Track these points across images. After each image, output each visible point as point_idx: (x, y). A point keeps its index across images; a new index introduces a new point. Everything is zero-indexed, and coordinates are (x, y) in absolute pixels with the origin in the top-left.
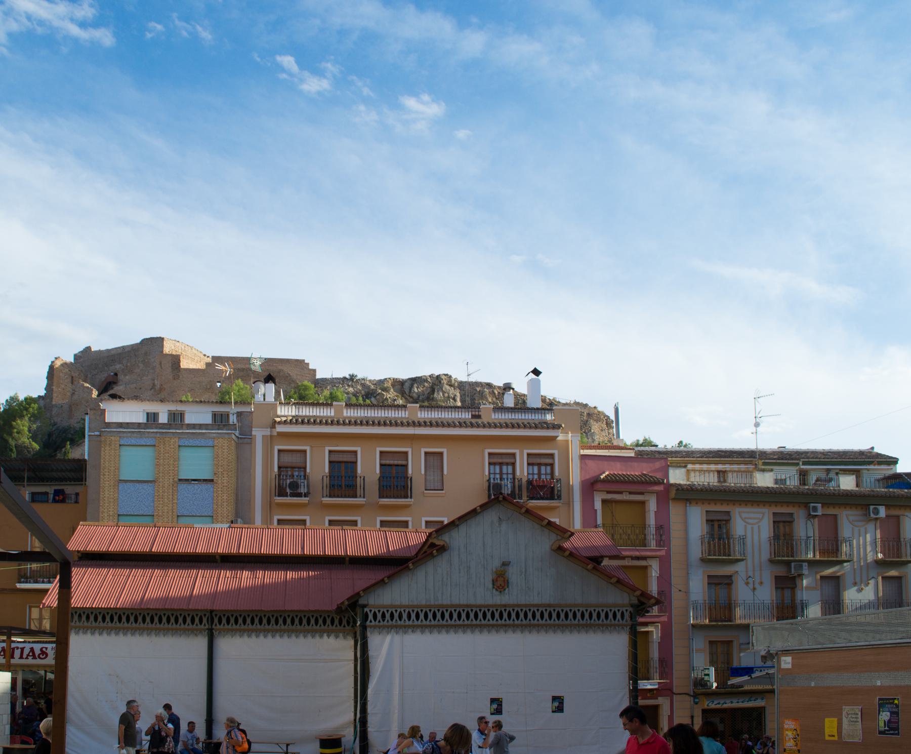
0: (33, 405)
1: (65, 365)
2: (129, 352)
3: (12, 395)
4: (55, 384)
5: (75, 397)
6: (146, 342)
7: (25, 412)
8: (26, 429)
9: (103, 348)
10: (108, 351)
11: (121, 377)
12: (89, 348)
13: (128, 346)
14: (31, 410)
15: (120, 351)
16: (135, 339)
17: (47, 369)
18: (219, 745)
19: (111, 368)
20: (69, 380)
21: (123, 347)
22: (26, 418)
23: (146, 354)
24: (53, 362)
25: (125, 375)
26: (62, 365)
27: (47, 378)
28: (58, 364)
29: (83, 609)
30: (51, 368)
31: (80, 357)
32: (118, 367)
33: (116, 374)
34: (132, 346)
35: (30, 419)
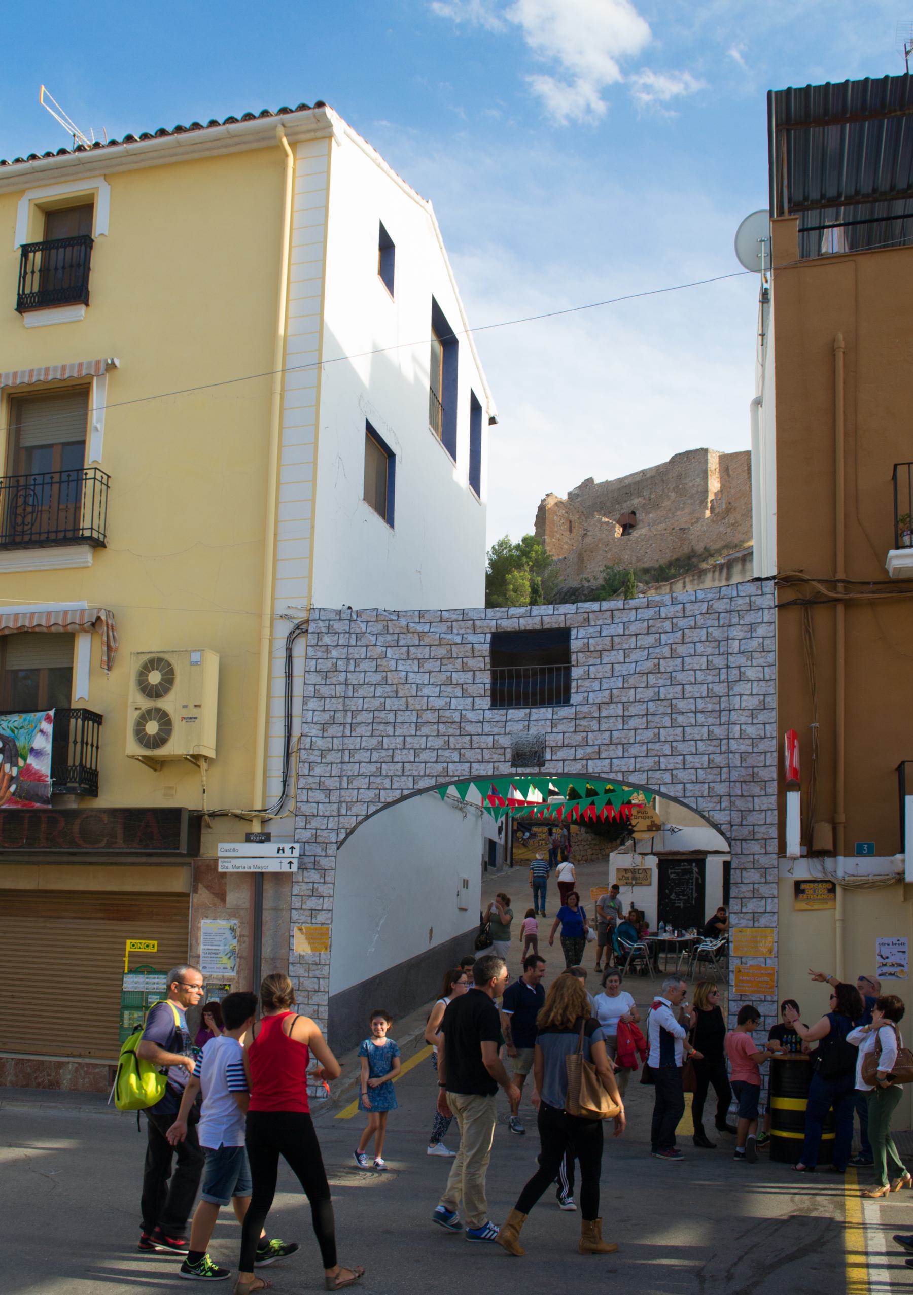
0: (536, 547)
1: (559, 504)
2: (652, 477)
3: (501, 537)
4: (547, 532)
5: (588, 540)
6: (678, 459)
7: (524, 559)
8: (527, 583)
9: (612, 477)
10: (620, 480)
11: (640, 516)
12: (590, 481)
13: (650, 469)
14: (533, 554)
15: (638, 478)
16: (661, 456)
17: (535, 512)
18: (907, 1262)
19: (625, 505)
20: (567, 526)
21: (643, 472)
22: (527, 568)
23: (680, 477)
24: (543, 501)
25: (648, 513)
26: (556, 504)
27: (535, 525)
28: (551, 503)
29: (349, 615)
30: (542, 509)
31: (577, 495)
32: (636, 501)
33: (633, 513)
34: (658, 467)
35: (531, 570)
